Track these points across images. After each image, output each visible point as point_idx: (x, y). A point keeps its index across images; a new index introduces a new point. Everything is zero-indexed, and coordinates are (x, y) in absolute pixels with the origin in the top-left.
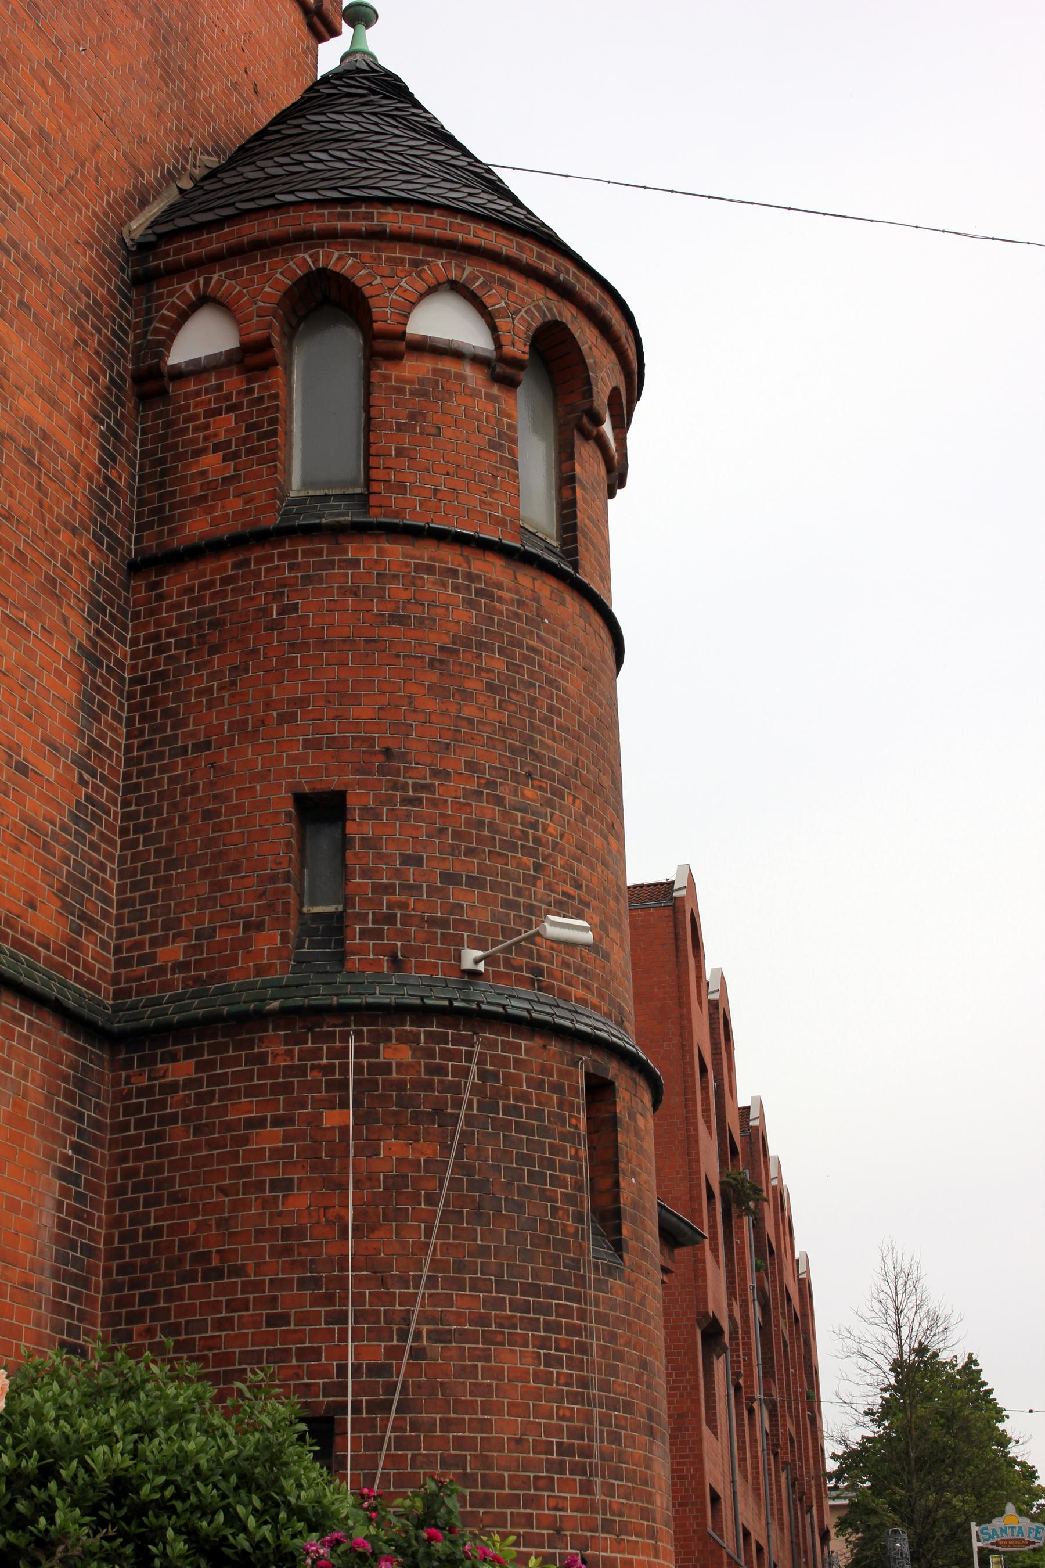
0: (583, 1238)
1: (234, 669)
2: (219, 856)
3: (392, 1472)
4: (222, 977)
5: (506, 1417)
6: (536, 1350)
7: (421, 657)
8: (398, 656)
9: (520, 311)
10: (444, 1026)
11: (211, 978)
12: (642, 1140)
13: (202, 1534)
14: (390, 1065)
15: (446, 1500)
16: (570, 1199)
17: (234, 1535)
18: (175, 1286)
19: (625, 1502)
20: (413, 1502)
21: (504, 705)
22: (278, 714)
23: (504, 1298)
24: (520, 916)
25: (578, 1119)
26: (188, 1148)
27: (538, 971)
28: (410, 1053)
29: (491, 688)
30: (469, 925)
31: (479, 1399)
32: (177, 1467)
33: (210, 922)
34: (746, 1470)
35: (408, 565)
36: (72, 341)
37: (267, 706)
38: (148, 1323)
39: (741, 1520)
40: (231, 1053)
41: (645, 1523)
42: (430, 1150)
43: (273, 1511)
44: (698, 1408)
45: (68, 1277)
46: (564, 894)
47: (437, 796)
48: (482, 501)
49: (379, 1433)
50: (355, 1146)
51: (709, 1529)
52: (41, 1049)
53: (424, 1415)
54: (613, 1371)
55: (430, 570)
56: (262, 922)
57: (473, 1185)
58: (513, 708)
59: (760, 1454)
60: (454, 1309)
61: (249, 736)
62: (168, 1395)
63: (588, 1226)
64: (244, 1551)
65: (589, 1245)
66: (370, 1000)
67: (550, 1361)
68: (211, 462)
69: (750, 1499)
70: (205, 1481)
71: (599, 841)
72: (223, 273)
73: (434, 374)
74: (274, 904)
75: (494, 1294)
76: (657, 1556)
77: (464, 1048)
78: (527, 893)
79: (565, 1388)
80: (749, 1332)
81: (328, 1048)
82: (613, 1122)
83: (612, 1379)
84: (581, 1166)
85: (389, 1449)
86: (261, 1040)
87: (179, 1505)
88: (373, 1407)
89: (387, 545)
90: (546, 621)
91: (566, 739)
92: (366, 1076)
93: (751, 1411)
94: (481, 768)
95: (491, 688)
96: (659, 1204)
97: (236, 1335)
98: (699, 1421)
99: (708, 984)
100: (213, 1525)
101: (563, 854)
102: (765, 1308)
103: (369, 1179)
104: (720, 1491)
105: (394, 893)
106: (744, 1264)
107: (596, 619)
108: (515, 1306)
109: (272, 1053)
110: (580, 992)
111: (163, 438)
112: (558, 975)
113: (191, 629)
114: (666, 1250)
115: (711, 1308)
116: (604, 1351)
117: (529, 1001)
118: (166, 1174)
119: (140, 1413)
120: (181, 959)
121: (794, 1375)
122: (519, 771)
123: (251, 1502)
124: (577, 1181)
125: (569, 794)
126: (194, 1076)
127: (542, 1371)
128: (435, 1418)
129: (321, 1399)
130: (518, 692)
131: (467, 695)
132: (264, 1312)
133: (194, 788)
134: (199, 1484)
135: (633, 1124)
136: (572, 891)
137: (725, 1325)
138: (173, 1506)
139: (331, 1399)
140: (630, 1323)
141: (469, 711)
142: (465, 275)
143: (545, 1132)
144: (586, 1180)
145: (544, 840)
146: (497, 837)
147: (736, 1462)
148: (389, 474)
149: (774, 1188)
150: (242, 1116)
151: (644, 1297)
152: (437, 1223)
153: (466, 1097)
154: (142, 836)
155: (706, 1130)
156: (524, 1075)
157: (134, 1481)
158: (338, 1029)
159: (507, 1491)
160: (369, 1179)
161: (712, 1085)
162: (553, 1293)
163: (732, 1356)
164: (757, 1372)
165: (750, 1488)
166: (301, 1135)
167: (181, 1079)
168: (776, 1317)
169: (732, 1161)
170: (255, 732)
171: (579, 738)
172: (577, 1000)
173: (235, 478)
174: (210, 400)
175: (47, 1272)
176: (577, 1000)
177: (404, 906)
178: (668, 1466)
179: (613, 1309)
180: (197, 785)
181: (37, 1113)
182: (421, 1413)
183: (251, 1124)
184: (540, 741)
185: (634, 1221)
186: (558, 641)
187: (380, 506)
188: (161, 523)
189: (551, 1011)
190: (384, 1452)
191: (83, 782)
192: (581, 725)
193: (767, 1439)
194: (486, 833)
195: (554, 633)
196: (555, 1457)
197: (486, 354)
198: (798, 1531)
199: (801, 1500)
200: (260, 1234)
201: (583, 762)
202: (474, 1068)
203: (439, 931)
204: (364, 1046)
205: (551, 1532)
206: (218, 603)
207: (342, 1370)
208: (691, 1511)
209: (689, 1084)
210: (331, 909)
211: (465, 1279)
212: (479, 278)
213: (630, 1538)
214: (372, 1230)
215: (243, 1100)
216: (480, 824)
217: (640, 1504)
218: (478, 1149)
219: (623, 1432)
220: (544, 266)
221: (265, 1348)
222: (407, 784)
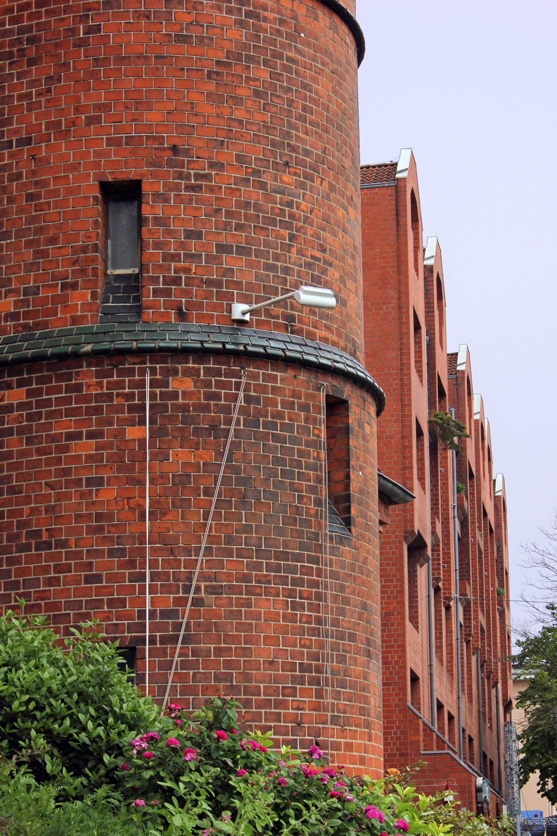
0: (321, 518)
1: (49, 79)
2: (40, 230)
3: (179, 685)
4: (46, 325)
5: (262, 646)
7: (201, 70)
8: (183, 69)
10: (219, 363)
11: (37, 326)
12: (368, 442)
13: (55, 733)
14: (177, 392)
15: (228, 710)
16: (313, 490)
17: (77, 734)
18: (14, 555)
19: (348, 703)
20: (206, 713)
21: (267, 108)
22: (86, 117)
23: (262, 562)
24: (278, 276)
25: (320, 430)
26: (22, 454)
27: (291, 318)
28: (192, 383)
29: (257, 93)
30: (238, 285)
31: (243, 634)
32: (36, 689)
33: (35, 282)
34: (442, 656)
37: (77, 110)
39: (436, 695)
40: (54, 384)
41: (363, 717)
42: (208, 455)
43: (104, 717)
44: (403, 608)
46: (313, 257)
47: (213, 184)
49: (169, 658)
50: (151, 453)
51: (409, 704)
53: (202, 645)
54: (342, 612)
57: (239, 481)
58: (274, 109)
59: (454, 642)
60: (225, 571)
61: (64, 135)
62: (27, 640)
63: (325, 509)
64: (84, 744)
65: (326, 522)
66: (162, 344)
67: (295, 606)
69: (445, 679)
70: (55, 697)
71: (340, 212)
74: (85, 269)
75: (255, 560)
76: (370, 740)
77: (234, 380)
78: (283, 258)
79: (306, 625)
80: (449, 544)
81: (129, 380)
82: (347, 430)
83: (341, 618)
84: (321, 465)
85: (176, 669)
86: (77, 374)
87: (38, 714)
88: (165, 640)
90: (302, 35)
91: (316, 133)
92: (159, 401)
93: (448, 608)
94: (249, 160)
95: (257, 93)
96: (379, 475)
97: (62, 590)
98: (403, 619)
99: (424, 250)
100: (63, 727)
101: (312, 225)
102: (464, 523)
103: (162, 477)
104: (419, 673)
105: (179, 261)
106: (447, 488)
107: (343, 29)
108: (269, 568)
109: (86, 384)
110: (324, 333)
112: (306, 320)
114: (383, 508)
115: (417, 526)
116: (335, 598)
117: (284, 342)
118: (5, 473)
119: (7, 653)
120: (12, 310)
121: (487, 577)
122: (278, 161)
123: (88, 712)
124: (318, 476)
125: (318, 177)
126: (26, 400)
127: (289, 613)
128: (210, 648)
129: (126, 634)
130: (279, 97)
131: (238, 101)
132: (83, 573)
133: (19, 176)
134: (52, 700)
135: (361, 431)
136: (319, 254)
137: (428, 540)
138: (35, 715)
139: (133, 634)
140: (355, 578)
141: (239, 114)
143: (294, 440)
144: (324, 475)
145: (297, 216)
146: (261, 215)
147: (434, 649)
149: (476, 421)
150: (64, 431)
151: (366, 558)
152: (213, 509)
153: (235, 416)
155: (418, 379)
156: (279, 399)
157: (7, 699)
158: (137, 366)
159: (262, 697)
160: (162, 477)
161: (424, 339)
162: (299, 558)
163: (433, 565)
164: (455, 576)
165: (445, 670)
166: (110, 446)
167: (15, 402)
168: (473, 530)
169: (440, 402)
171: (326, 131)
172: (321, 339)
176: (321, 339)
177: (187, 270)
178: (381, 677)
179: (343, 568)
182: (200, 644)
183: (70, 436)
184: (296, 135)
185: (360, 503)
186: (312, 51)
189: (301, 350)
190: (173, 671)
192: (329, 120)
193: (461, 630)
194: (252, 212)
195: (308, 45)
196: (298, 673)
198: (484, 703)
199: (488, 678)
201: (329, 150)
202: (242, 395)
203: (215, 290)
204: (157, 379)
205: (294, 725)
206: (34, 22)
207: (142, 614)
208: (394, 689)
209: (404, 320)
210: (129, 271)
211: (233, 549)
213: (351, 728)
214: (164, 514)
215: (64, 419)
216: (247, 205)
217: (359, 704)
218: (244, 454)
219: (348, 655)
221: (84, 599)
222: (190, 173)
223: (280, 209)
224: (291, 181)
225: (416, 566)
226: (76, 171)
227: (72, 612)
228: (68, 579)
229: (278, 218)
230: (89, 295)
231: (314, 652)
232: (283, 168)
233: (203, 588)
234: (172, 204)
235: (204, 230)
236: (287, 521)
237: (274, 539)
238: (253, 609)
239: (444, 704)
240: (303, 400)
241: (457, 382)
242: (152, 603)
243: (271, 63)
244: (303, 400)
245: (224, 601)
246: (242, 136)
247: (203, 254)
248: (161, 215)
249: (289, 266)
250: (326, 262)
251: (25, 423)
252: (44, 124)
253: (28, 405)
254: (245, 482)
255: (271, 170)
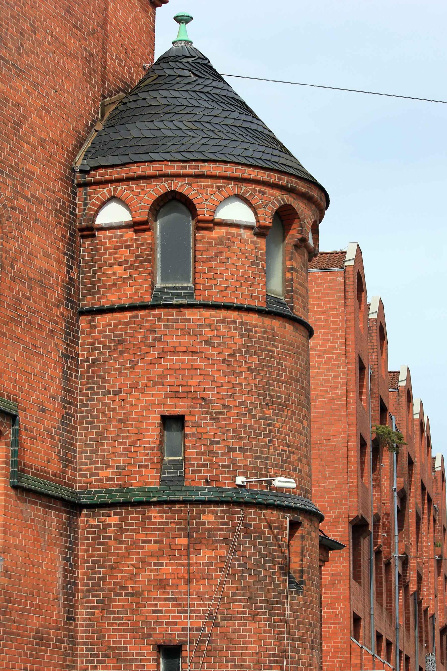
6: (265, 622)
9: (269, 203)
21: (257, 377)
29: (251, 370)
31: (241, 639)
35: (213, 320)
36: (55, 225)
38: (101, 610)
40: (135, 515)
45: (68, 594)
46: (282, 450)
47: (226, 416)
48: (248, 290)
52: (56, 515)
55: (224, 322)
56: (148, 465)
58: (261, 377)
60: (231, 609)
67: (270, 626)
68: (118, 270)
72: (123, 187)
73: (226, 235)
74: (153, 459)
75: (248, 604)
77: (237, 515)
78: (265, 452)
79: (277, 635)
86: (148, 511)
89: (204, 312)
92: (195, 526)
94: (246, 404)
95: (251, 370)
97: (140, 616)
111: (94, 255)
113: (110, 342)
120: (110, 476)
122: (263, 403)
129: (176, 639)
131: (240, 374)
133: (114, 409)
140: (305, 611)
142: (242, 191)
145: (273, 430)
146: (253, 431)
148: (205, 281)
150: (141, 539)
154: (89, 426)
158: (182, 508)
162: (272, 602)
165: (384, 610)
167: (112, 523)
170: (143, 388)
173: (130, 278)
174: (117, 241)
175: (61, 594)
179: (298, 606)
180: (116, 408)
181: (56, 539)
183: (144, 542)
187: (201, 295)
188: (94, 293)
191: (65, 408)
196: (272, 658)
197: (253, 225)
200: (149, 581)
203: (226, 470)
204: (194, 515)
212: (249, 191)
216: (245, 426)
218: (242, 552)
220: (281, 182)
221: (153, 621)
222: (212, 412)
223: (264, 428)
224: (270, 412)
225: (360, 538)
226: (147, 409)
227: (146, 627)
228: (143, 611)
229: (262, 432)
230: (155, 471)
231: (281, 648)
232: (266, 406)
233: (219, 617)
234: (202, 427)
235: (220, 440)
236: (266, 584)
237: (259, 593)
238: (247, 627)
239: (383, 634)
240: (276, 524)
241: (399, 394)
242: (191, 625)
243: (259, 354)
244: (276, 524)
245: (231, 624)
246: (242, 392)
247: (220, 452)
248: (196, 433)
249: (269, 456)
250: (289, 452)
251: (118, 534)
252: (129, 384)
253: (121, 525)
254: (244, 566)
255: (259, 408)
